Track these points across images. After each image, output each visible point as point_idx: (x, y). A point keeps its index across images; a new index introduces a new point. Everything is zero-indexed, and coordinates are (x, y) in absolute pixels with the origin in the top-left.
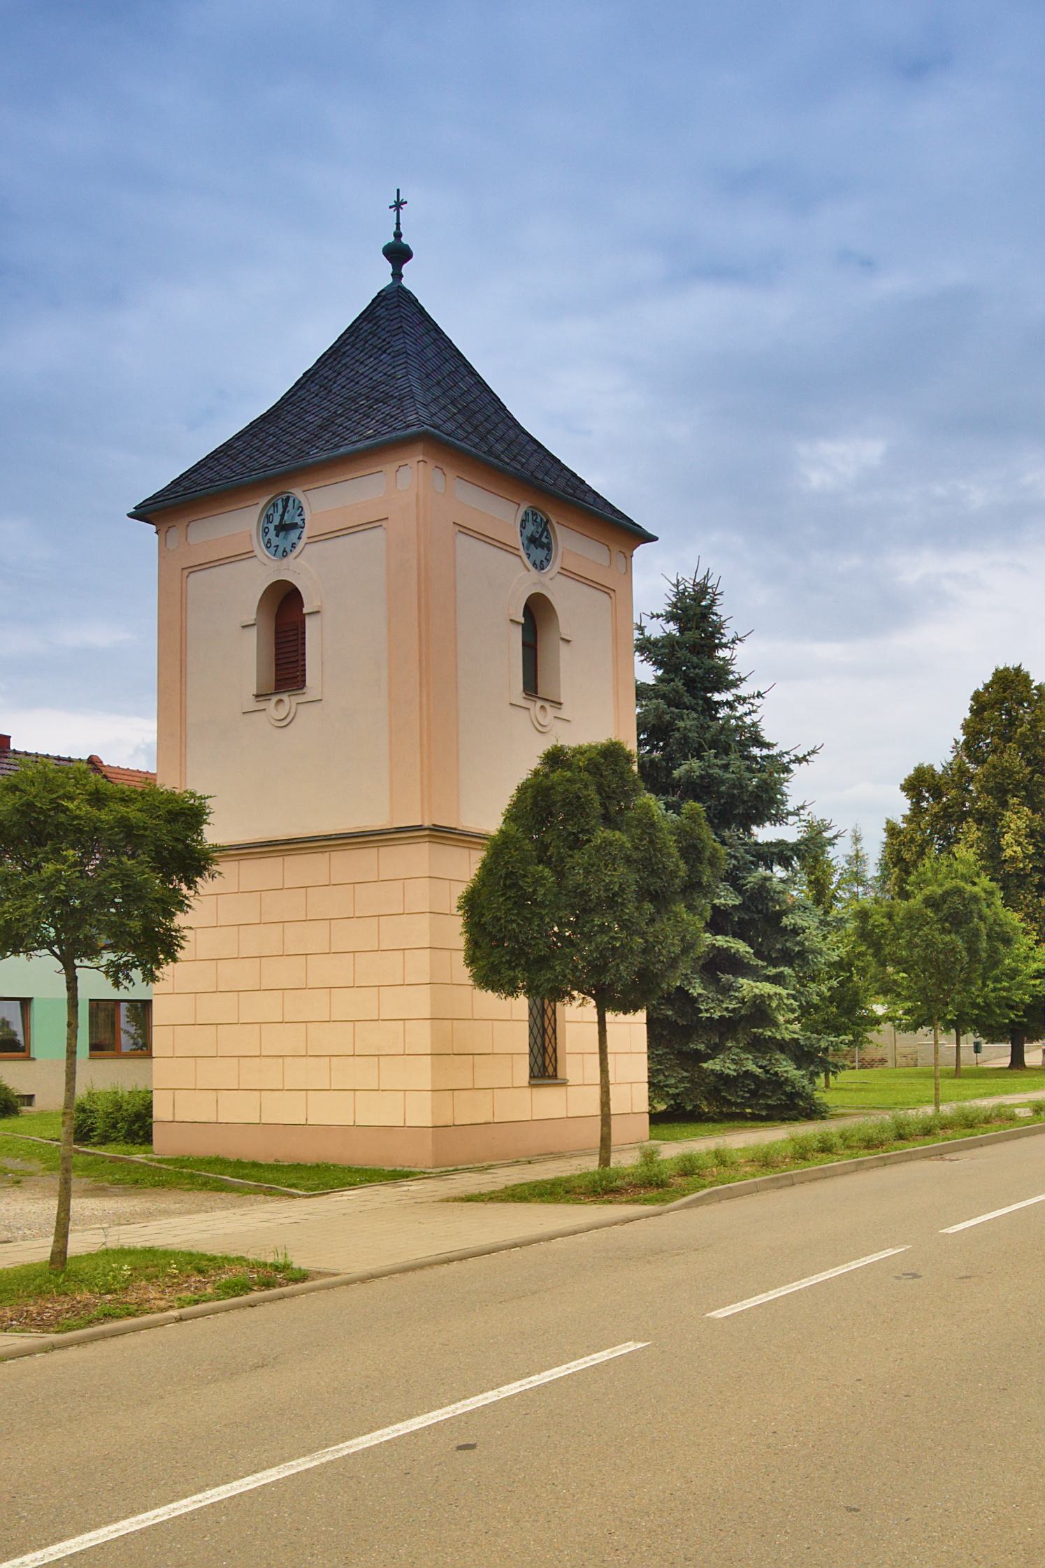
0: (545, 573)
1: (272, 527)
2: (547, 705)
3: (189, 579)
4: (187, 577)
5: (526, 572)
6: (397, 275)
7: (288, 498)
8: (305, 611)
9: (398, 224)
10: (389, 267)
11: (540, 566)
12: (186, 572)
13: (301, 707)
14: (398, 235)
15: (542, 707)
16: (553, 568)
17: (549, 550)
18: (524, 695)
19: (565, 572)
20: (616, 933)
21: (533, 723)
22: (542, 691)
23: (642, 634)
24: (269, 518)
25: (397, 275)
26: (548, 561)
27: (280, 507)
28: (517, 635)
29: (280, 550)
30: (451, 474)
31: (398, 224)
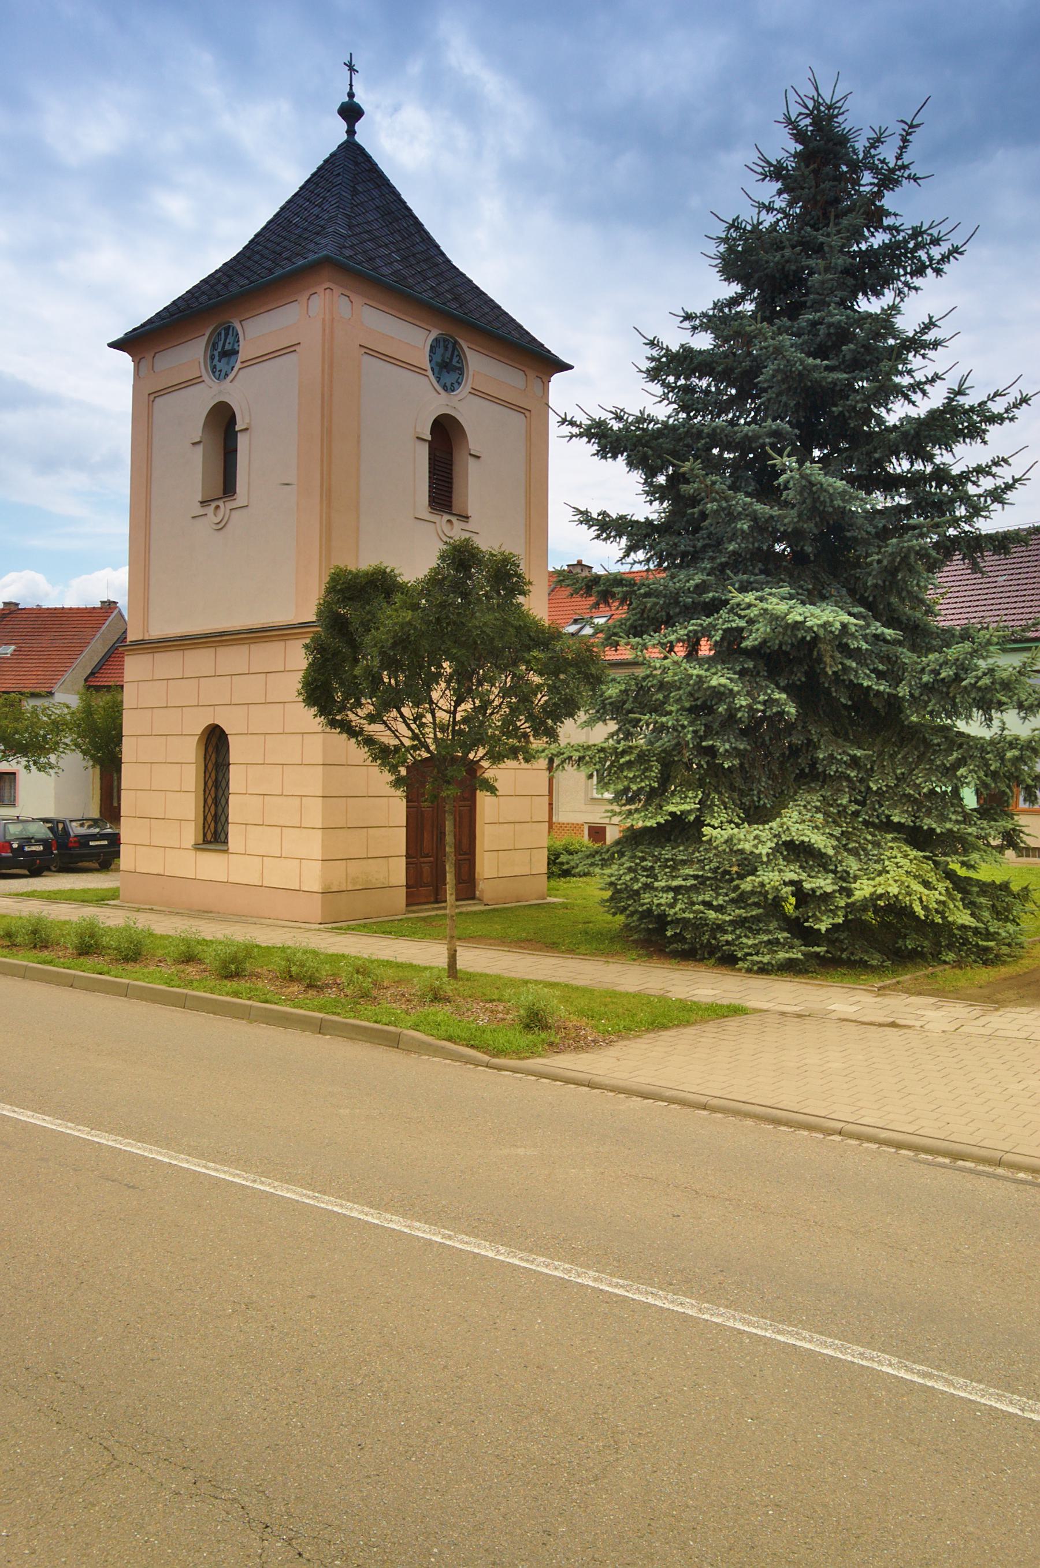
0: (456, 395)
1: (216, 353)
2: (454, 519)
3: (155, 402)
4: (153, 401)
5: (435, 394)
6: (351, 132)
7: (229, 326)
8: (237, 428)
9: (351, 85)
10: (343, 125)
11: (449, 388)
12: (152, 397)
13: (233, 512)
14: (351, 95)
15: (449, 521)
16: (463, 391)
17: (462, 374)
18: (430, 510)
19: (475, 392)
20: (967, 818)
21: (438, 535)
22: (457, 506)
23: (793, 506)
24: (214, 347)
25: (351, 132)
26: (459, 384)
27: (223, 335)
28: (423, 453)
29: (223, 374)
30: (358, 300)
31: (351, 85)
